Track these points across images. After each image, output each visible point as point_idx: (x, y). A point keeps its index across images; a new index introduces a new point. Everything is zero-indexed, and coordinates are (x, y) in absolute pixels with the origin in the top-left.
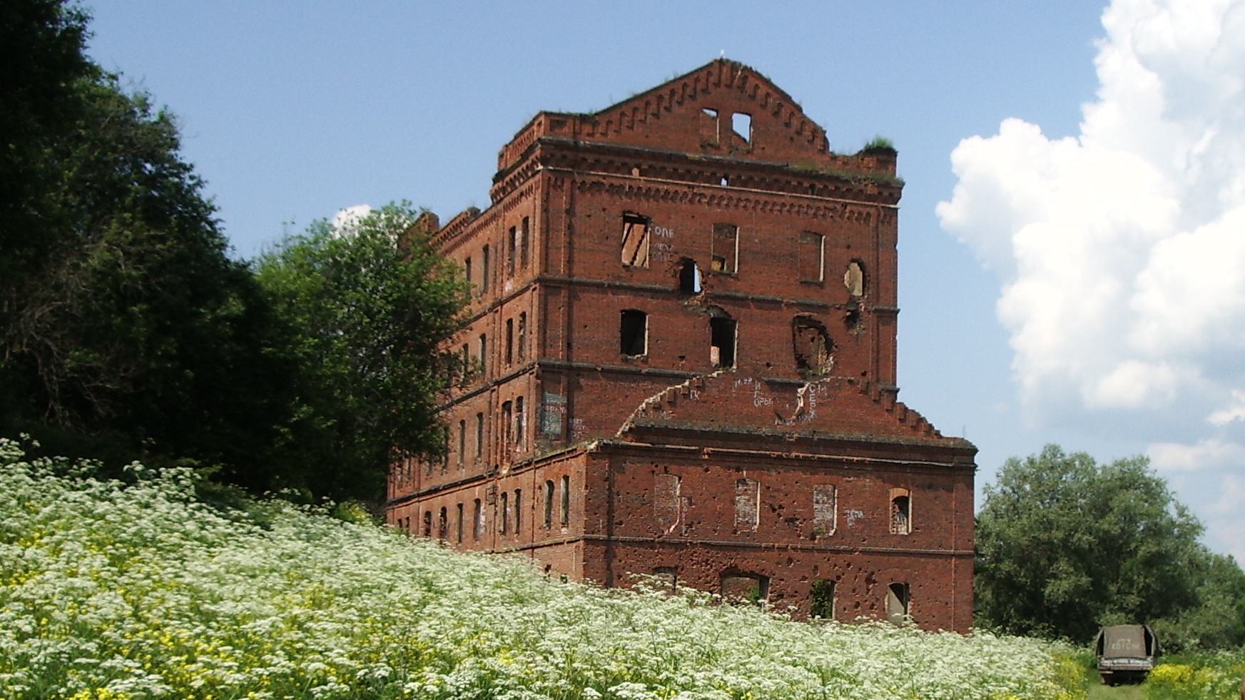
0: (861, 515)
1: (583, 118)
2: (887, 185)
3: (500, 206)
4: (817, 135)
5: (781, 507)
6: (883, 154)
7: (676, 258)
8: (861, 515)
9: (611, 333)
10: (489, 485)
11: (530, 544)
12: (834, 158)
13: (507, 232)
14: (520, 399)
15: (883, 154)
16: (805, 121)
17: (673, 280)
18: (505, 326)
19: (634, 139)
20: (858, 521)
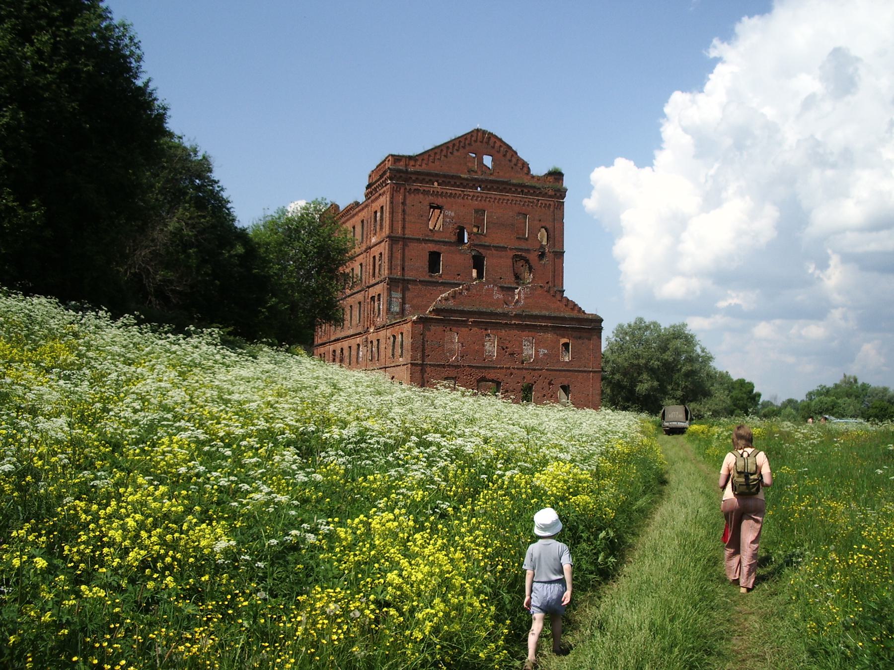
0: (546, 351)
1: (410, 158)
2: (559, 190)
3: (370, 201)
4: (525, 166)
5: (507, 348)
6: (556, 175)
7: (456, 226)
8: (546, 351)
9: (424, 263)
10: (364, 337)
11: (384, 366)
12: (533, 177)
13: (373, 213)
14: (379, 295)
15: (556, 175)
16: (519, 159)
17: (454, 237)
18: (372, 259)
19: (435, 167)
20: (545, 354)
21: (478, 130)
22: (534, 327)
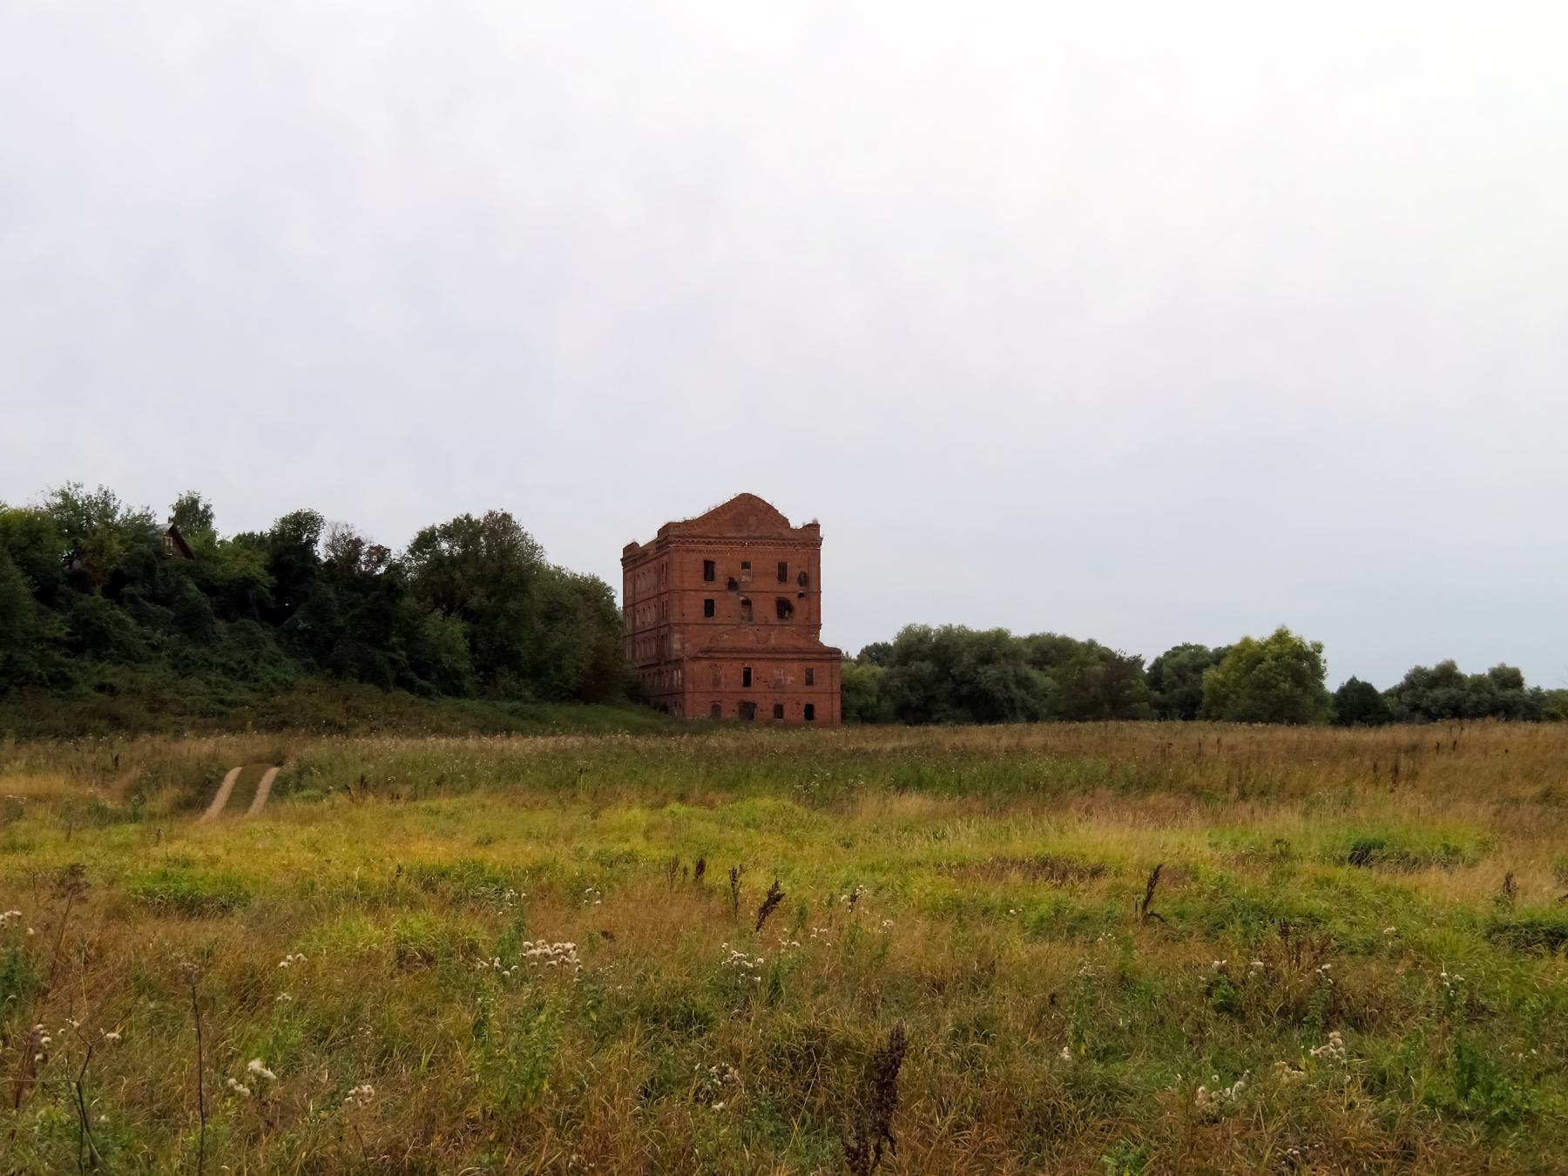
2: (815, 540)
4: (785, 521)
6: (814, 527)
12: (792, 530)
19: (697, 531)
21: (743, 495)
22: (783, 659)
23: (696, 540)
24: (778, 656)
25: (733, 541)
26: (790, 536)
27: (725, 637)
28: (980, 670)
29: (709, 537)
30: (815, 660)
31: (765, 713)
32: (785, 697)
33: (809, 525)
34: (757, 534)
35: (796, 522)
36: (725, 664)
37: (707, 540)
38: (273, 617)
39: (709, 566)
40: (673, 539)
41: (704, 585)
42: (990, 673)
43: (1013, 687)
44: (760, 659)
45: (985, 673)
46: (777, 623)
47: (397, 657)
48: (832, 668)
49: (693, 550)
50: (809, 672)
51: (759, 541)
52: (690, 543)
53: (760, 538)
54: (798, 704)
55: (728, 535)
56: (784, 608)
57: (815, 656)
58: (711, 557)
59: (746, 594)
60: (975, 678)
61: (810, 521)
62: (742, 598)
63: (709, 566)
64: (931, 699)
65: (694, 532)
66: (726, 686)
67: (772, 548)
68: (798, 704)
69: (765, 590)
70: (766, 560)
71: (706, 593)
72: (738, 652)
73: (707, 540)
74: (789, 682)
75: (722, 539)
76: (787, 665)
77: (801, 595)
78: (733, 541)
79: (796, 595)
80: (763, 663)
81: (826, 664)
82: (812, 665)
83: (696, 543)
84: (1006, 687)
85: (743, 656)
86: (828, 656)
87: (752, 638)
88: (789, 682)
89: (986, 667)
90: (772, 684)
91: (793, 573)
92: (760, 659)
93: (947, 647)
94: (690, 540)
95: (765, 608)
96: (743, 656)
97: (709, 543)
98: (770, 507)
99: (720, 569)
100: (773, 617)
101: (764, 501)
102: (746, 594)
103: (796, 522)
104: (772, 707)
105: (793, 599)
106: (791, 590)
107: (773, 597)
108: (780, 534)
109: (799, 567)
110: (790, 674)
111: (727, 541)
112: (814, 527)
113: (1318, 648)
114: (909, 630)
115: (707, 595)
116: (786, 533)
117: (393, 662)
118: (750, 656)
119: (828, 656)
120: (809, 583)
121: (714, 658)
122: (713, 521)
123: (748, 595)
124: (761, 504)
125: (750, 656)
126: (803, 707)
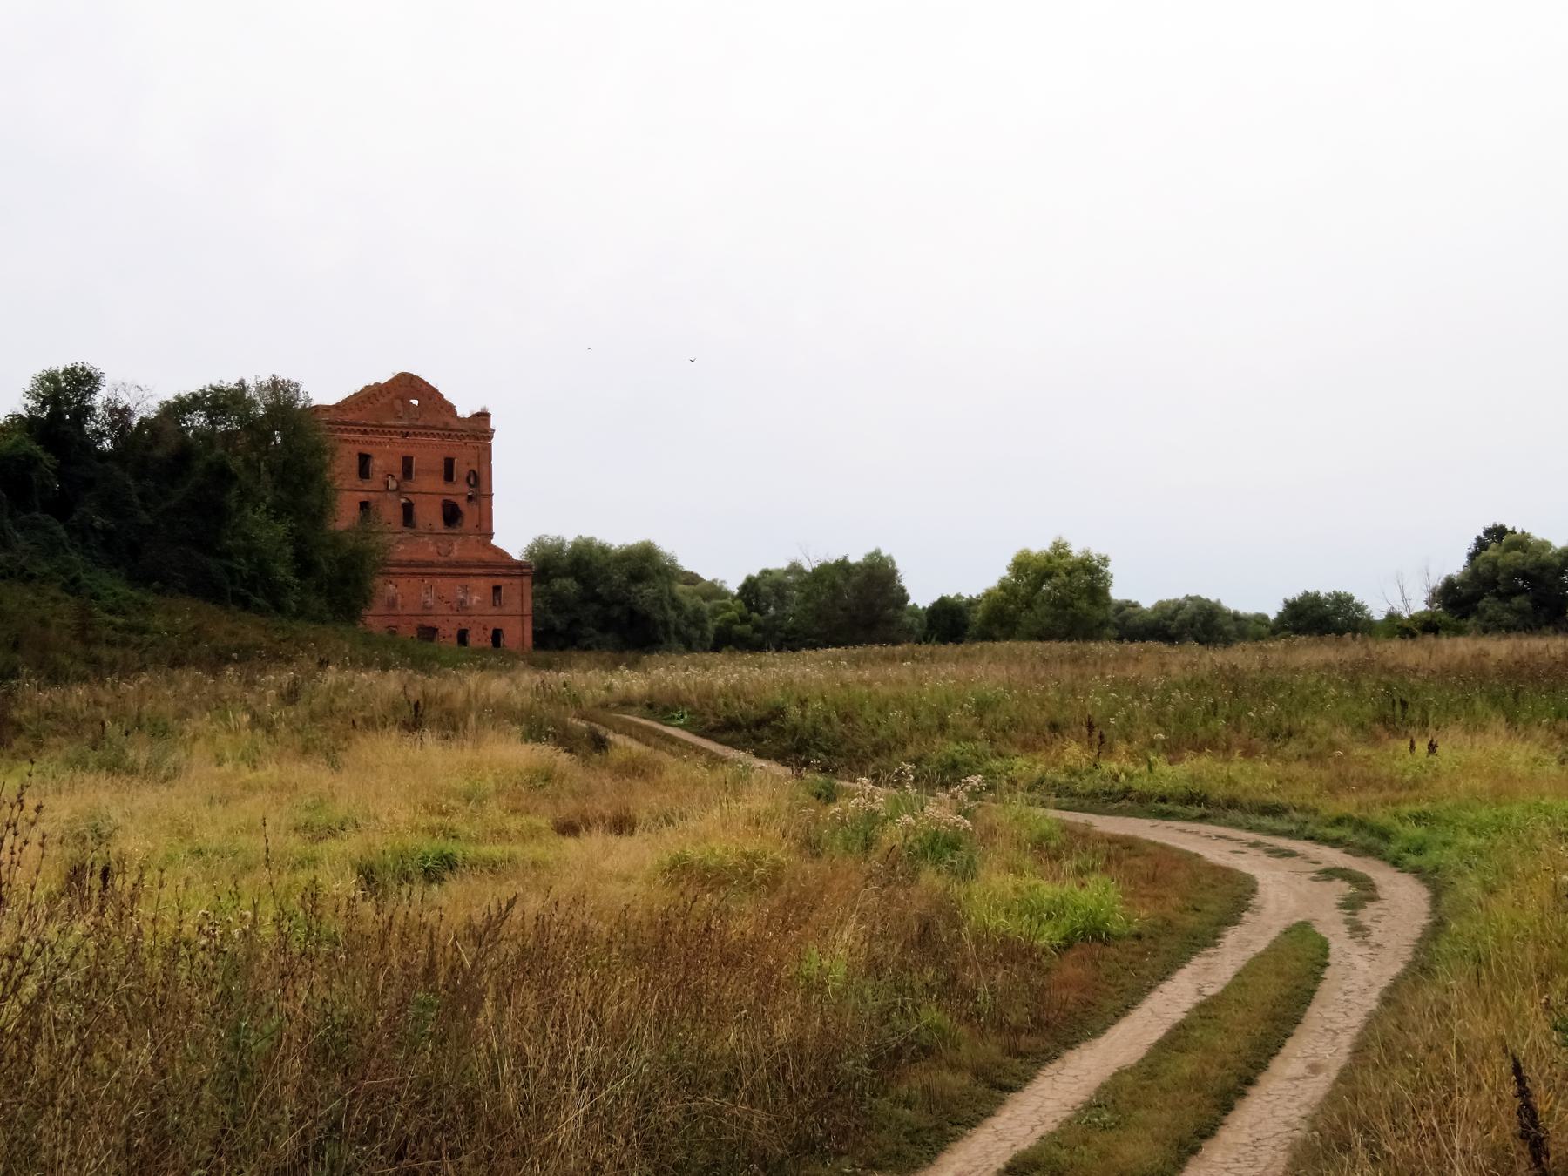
2: (486, 432)
4: (451, 409)
6: (483, 416)
12: (459, 419)
16: (446, 402)
19: (350, 417)
20: (478, 601)
21: (404, 374)
22: (468, 575)
23: (349, 428)
24: (462, 571)
25: (392, 430)
26: (458, 426)
27: (402, 547)
28: (634, 589)
29: (365, 425)
30: (505, 575)
31: (449, 640)
32: (471, 619)
33: (478, 415)
34: (419, 423)
35: (464, 410)
36: (403, 581)
37: (362, 429)
38: (61, 508)
39: (364, 459)
40: (323, 425)
41: (360, 483)
42: (645, 592)
43: (668, 608)
44: (442, 575)
45: (640, 591)
46: (443, 531)
47: (235, 566)
48: (522, 585)
49: (346, 440)
50: (497, 589)
51: (423, 431)
52: (342, 432)
53: (424, 427)
54: (485, 629)
55: (387, 423)
56: (451, 514)
57: (504, 571)
58: (368, 450)
59: (408, 496)
60: (629, 599)
61: (478, 410)
62: (403, 500)
63: (364, 459)
64: (575, 622)
65: (347, 418)
66: (403, 607)
67: (436, 440)
68: (485, 629)
69: (429, 490)
70: (427, 454)
71: (362, 494)
72: (418, 566)
73: (362, 429)
74: (474, 602)
75: (380, 428)
76: (473, 582)
77: (470, 498)
78: (392, 430)
79: (464, 498)
80: (445, 580)
81: (516, 581)
82: (499, 581)
83: (349, 432)
84: (662, 608)
85: (423, 570)
86: (517, 571)
87: (432, 549)
88: (474, 602)
89: (641, 586)
90: (455, 606)
91: (460, 470)
92: (442, 575)
93: (588, 563)
94: (343, 427)
95: (429, 514)
96: (423, 570)
97: (365, 432)
98: (435, 391)
99: (377, 464)
100: (439, 525)
101: (427, 384)
102: (408, 496)
103: (464, 410)
104: (455, 633)
105: (461, 502)
106: (458, 491)
107: (439, 500)
108: (447, 424)
109: (468, 464)
110: (477, 594)
111: (386, 430)
112: (483, 416)
113: (1105, 561)
114: (539, 543)
115: (362, 496)
116: (453, 424)
117: (229, 571)
118: (430, 570)
119: (517, 571)
120: (479, 484)
121: (389, 574)
122: (370, 406)
123: (411, 497)
124: (424, 387)
125: (430, 570)
126: (490, 633)
